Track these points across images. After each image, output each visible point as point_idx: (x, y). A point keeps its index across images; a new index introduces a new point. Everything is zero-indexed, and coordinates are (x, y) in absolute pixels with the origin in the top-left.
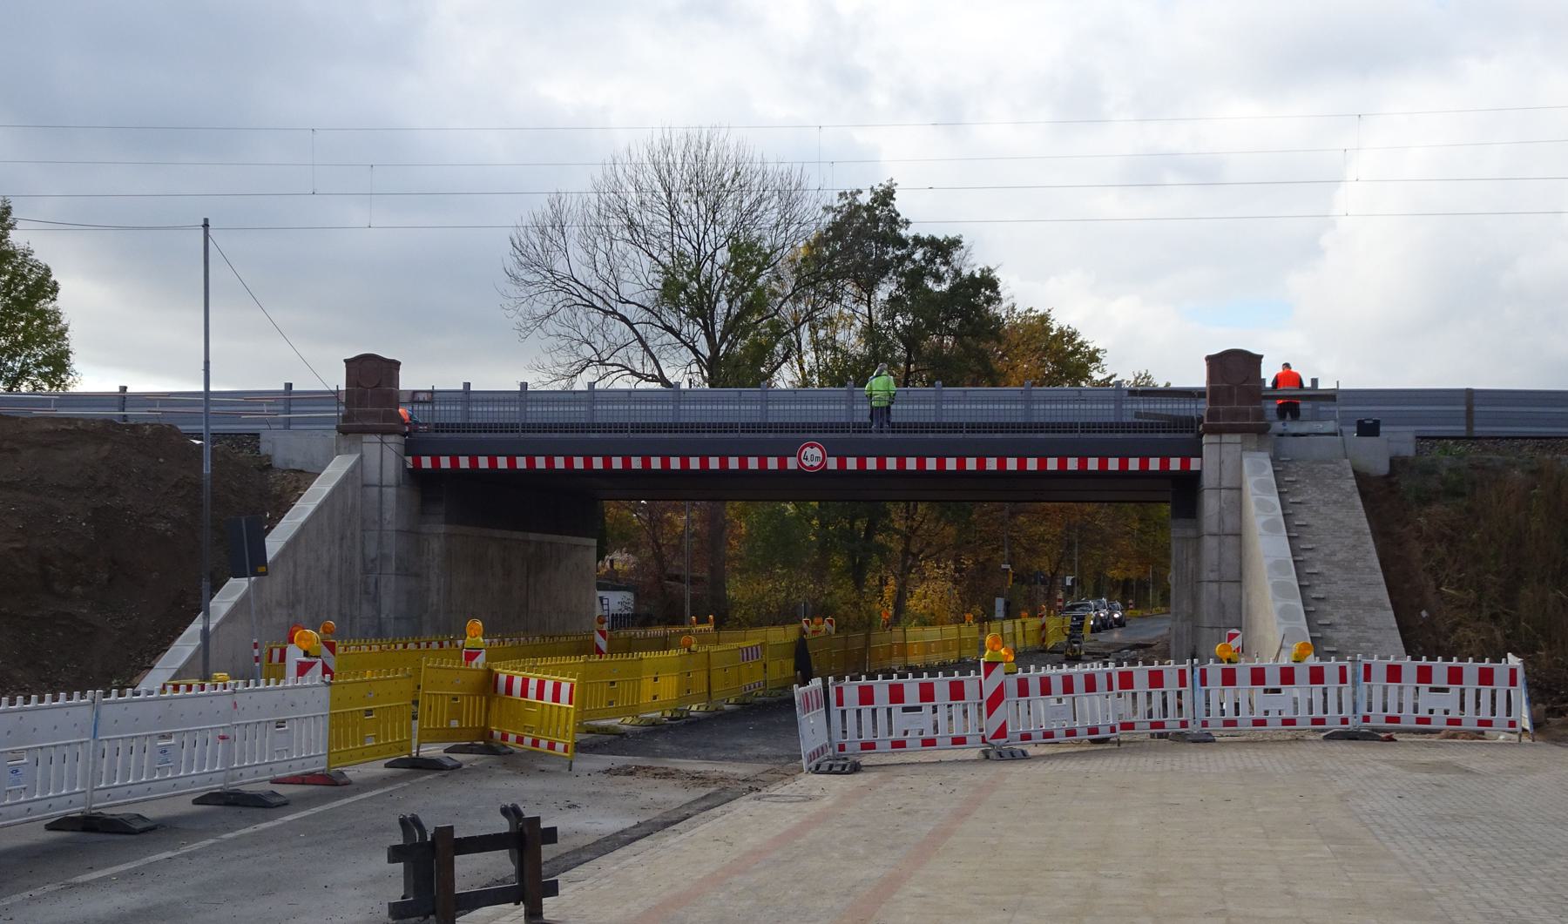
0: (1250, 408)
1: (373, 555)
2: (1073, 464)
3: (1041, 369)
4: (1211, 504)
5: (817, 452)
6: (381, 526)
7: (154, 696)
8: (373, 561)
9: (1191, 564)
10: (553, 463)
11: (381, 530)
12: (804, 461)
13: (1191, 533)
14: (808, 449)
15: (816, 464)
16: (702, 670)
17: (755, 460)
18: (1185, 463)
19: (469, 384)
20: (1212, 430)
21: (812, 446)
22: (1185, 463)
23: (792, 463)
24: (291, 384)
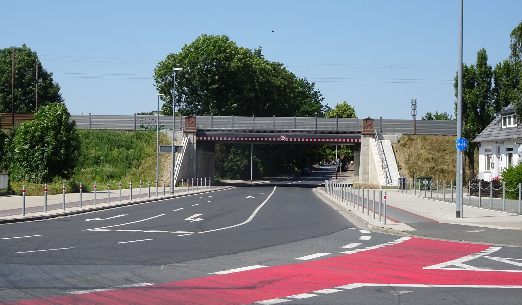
0: (371, 130)
1: (191, 158)
2: (327, 140)
3: (220, 80)
4: (362, 149)
5: (284, 137)
6: (193, 152)
7: (508, 116)
8: (192, 159)
9: (358, 161)
10: (216, 139)
11: (193, 153)
12: (281, 139)
13: (358, 154)
14: (282, 136)
15: (284, 140)
16: (381, 142)
17: (340, 139)
18: (358, 140)
19: (486, 152)
20: (365, 135)
21: (283, 136)
22: (358, 140)
23: (278, 140)
24: (91, 114)
